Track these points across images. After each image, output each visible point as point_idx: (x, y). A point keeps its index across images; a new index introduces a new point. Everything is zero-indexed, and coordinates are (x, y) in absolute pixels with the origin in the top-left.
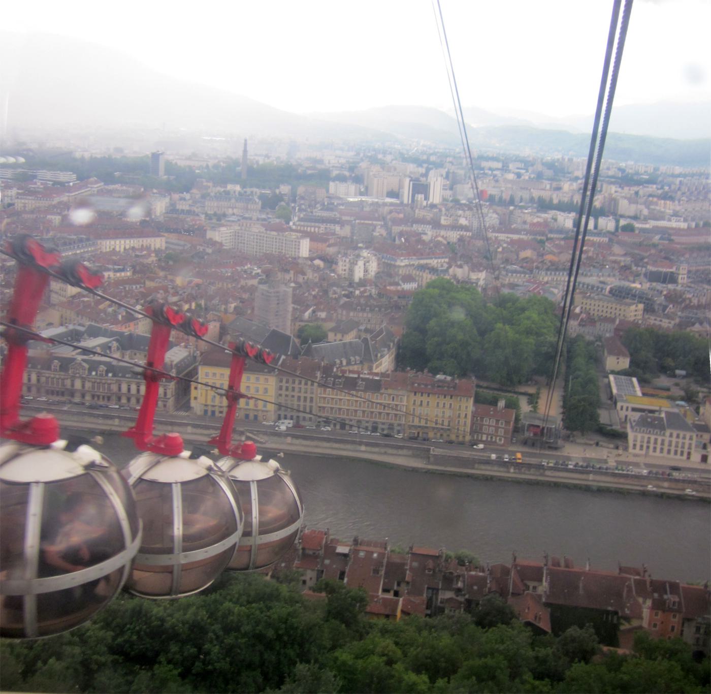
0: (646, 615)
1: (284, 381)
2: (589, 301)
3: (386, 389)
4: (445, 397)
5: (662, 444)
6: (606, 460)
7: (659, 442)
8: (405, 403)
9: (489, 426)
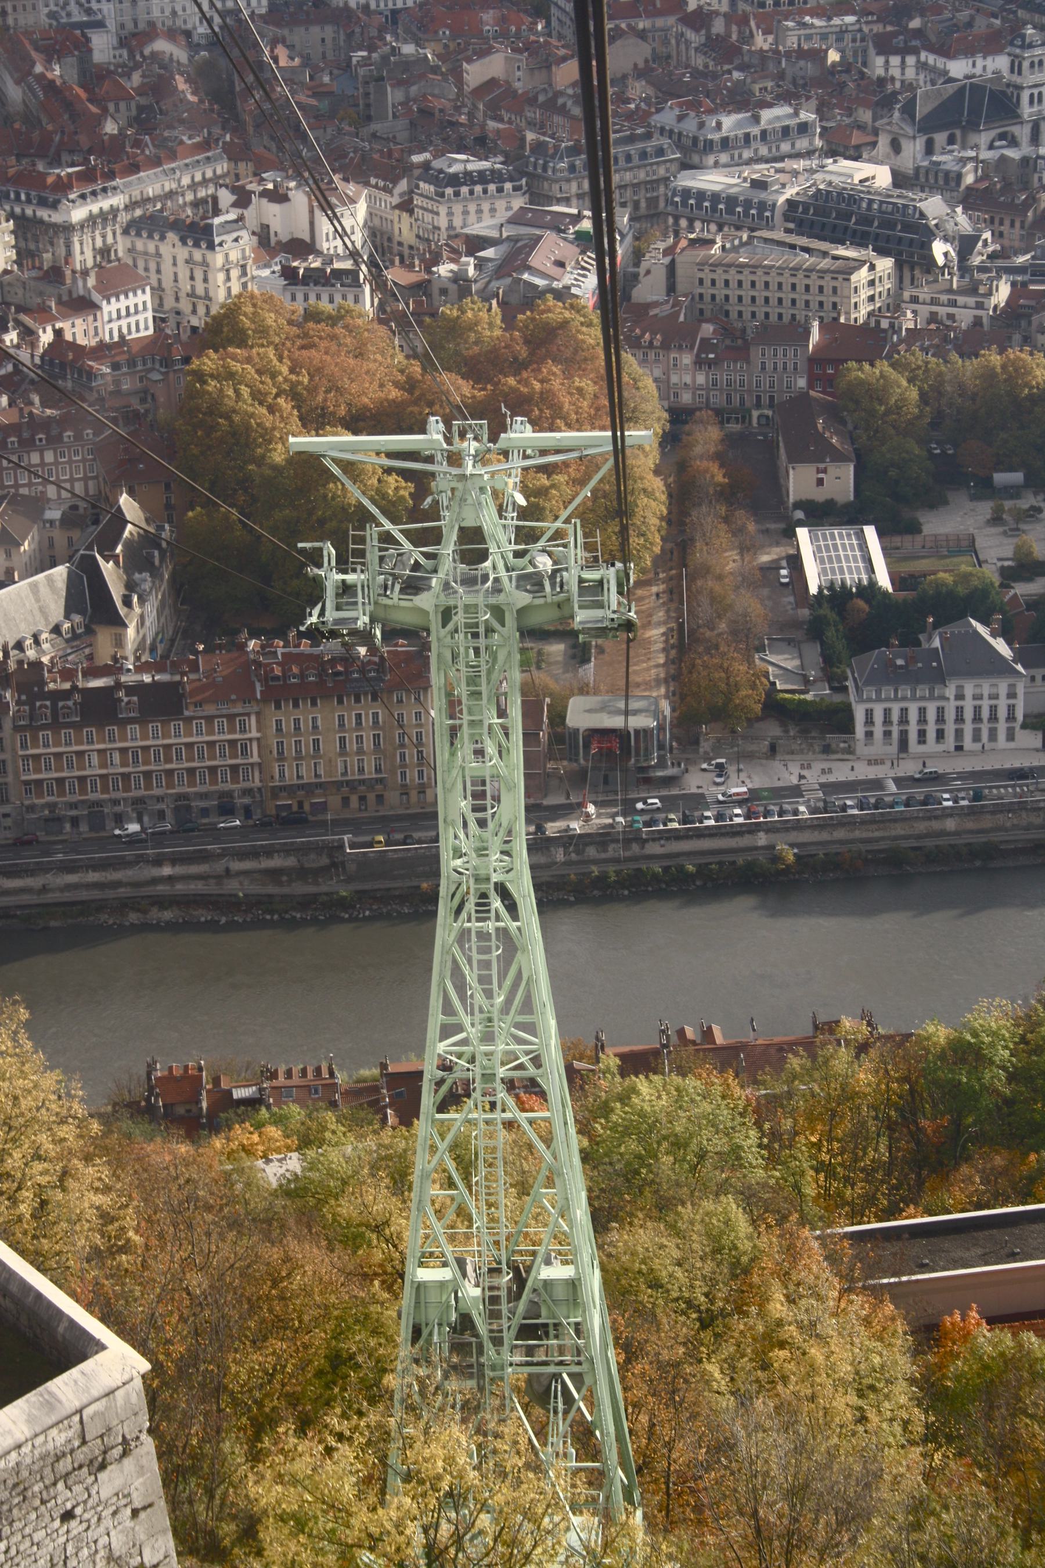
0: (817, 748)
3: (199, 704)
5: (940, 719)
6: (798, 786)
7: (931, 716)
8: (254, 734)
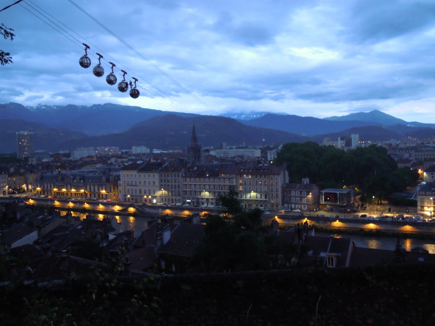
1: (163, 175)
2: (420, 154)
4: (261, 177)
9: (295, 197)
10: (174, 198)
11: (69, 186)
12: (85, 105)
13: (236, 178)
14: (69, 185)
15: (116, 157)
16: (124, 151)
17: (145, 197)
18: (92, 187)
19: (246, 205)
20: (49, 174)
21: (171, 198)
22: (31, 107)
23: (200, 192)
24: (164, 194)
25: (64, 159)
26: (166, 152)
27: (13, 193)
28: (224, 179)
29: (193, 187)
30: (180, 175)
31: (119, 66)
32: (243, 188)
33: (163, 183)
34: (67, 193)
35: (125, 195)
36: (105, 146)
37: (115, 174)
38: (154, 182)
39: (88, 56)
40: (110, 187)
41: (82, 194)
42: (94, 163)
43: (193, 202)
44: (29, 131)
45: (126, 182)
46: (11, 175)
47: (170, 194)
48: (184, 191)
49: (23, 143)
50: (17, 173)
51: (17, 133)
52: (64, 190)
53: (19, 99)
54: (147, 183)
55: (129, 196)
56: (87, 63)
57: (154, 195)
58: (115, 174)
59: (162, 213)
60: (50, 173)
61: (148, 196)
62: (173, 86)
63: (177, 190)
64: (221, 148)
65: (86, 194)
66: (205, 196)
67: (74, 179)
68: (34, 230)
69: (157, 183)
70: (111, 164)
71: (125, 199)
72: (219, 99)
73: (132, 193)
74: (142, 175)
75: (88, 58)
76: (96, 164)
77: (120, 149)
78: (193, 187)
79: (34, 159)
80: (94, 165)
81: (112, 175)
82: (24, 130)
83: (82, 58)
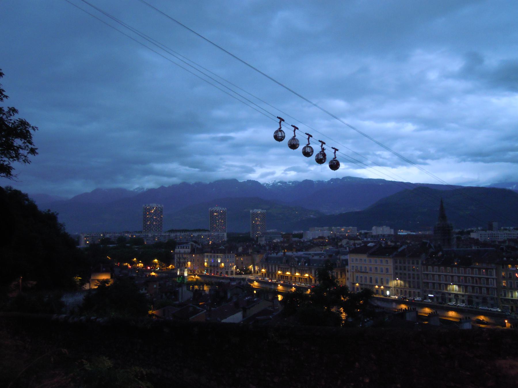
10: (412, 291)
11: (293, 269)
12: (321, 180)
13: (496, 269)
14: (294, 268)
15: (348, 239)
16: (363, 232)
17: (377, 287)
18: (273, 267)
19: (512, 307)
20: (274, 255)
21: (408, 291)
22: (267, 184)
23: (446, 285)
24: (399, 285)
25: (296, 239)
26: (414, 233)
27: (240, 274)
28: (479, 269)
29: (436, 277)
30: (420, 262)
31: (316, 136)
32: (507, 283)
33: (399, 271)
34: (291, 277)
35: (354, 284)
36: (342, 226)
37: (343, 257)
38: (387, 269)
39: (282, 129)
40: (337, 273)
41: (306, 279)
42: (324, 244)
43: (437, 298)
44: (262, 209)
45: (355, 268)
46: (239, 255)
47: (407, 285)
48: (424, 283)
49: (256, 221)
50: (245, 253)
51: (251, 211)
52: (288, 273)
53: (253, 176)
54: (379, 271)
55: (357, 284)
56: (282, 137)
57: (387, 285)
58: (343, 257)
59: (396, 309)
60: (275, 254)
61: (379, 286)
62: (418, 153)
63: (416, 280)
64: (491, 228)
65: (311, 280)
66: (453, 290)
67: (298, 262)
68: (239, 311)
69: (391, 271)
70: (341, 246)
71: (354, 288)
72: (481, 164)
73: (361, 281)
74: (373, 259)
75: (282, 131)
76: (326, 245)
77: (358, 231)
78: (436, 277)
79: (264, 239)
80: (324, 247)
81: (339, 259)
82: (257, 208)
83: (276, 132)
